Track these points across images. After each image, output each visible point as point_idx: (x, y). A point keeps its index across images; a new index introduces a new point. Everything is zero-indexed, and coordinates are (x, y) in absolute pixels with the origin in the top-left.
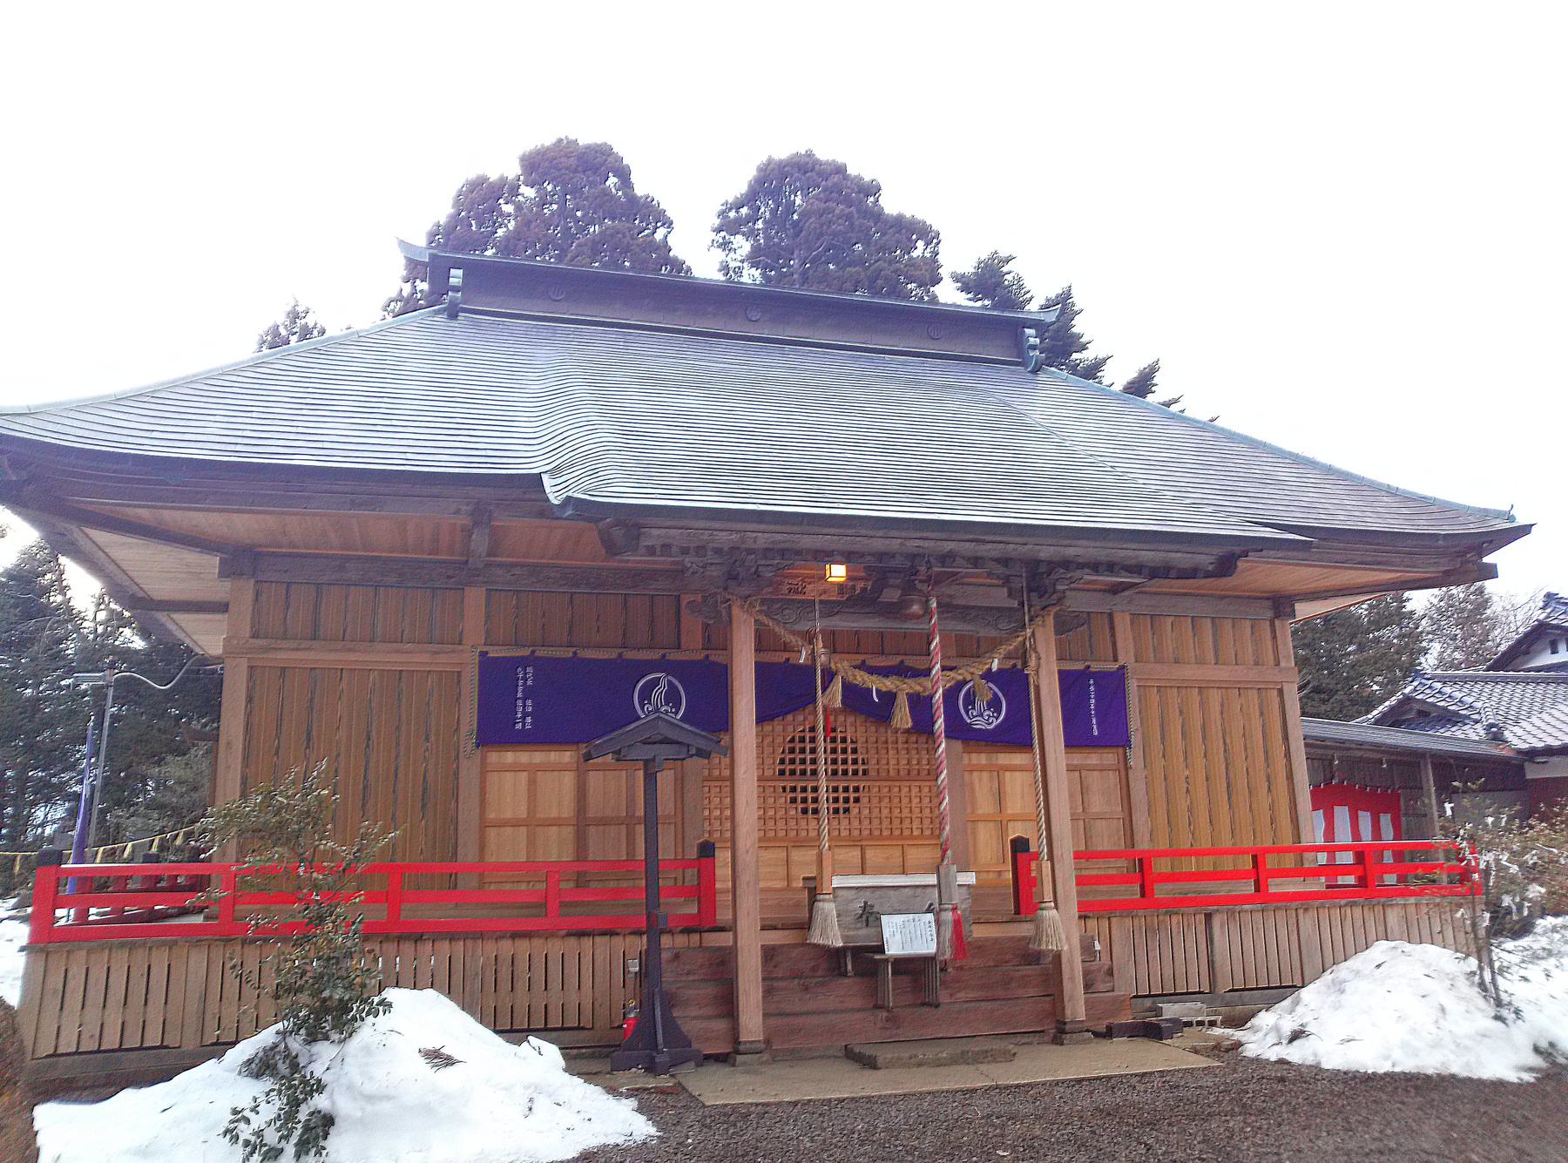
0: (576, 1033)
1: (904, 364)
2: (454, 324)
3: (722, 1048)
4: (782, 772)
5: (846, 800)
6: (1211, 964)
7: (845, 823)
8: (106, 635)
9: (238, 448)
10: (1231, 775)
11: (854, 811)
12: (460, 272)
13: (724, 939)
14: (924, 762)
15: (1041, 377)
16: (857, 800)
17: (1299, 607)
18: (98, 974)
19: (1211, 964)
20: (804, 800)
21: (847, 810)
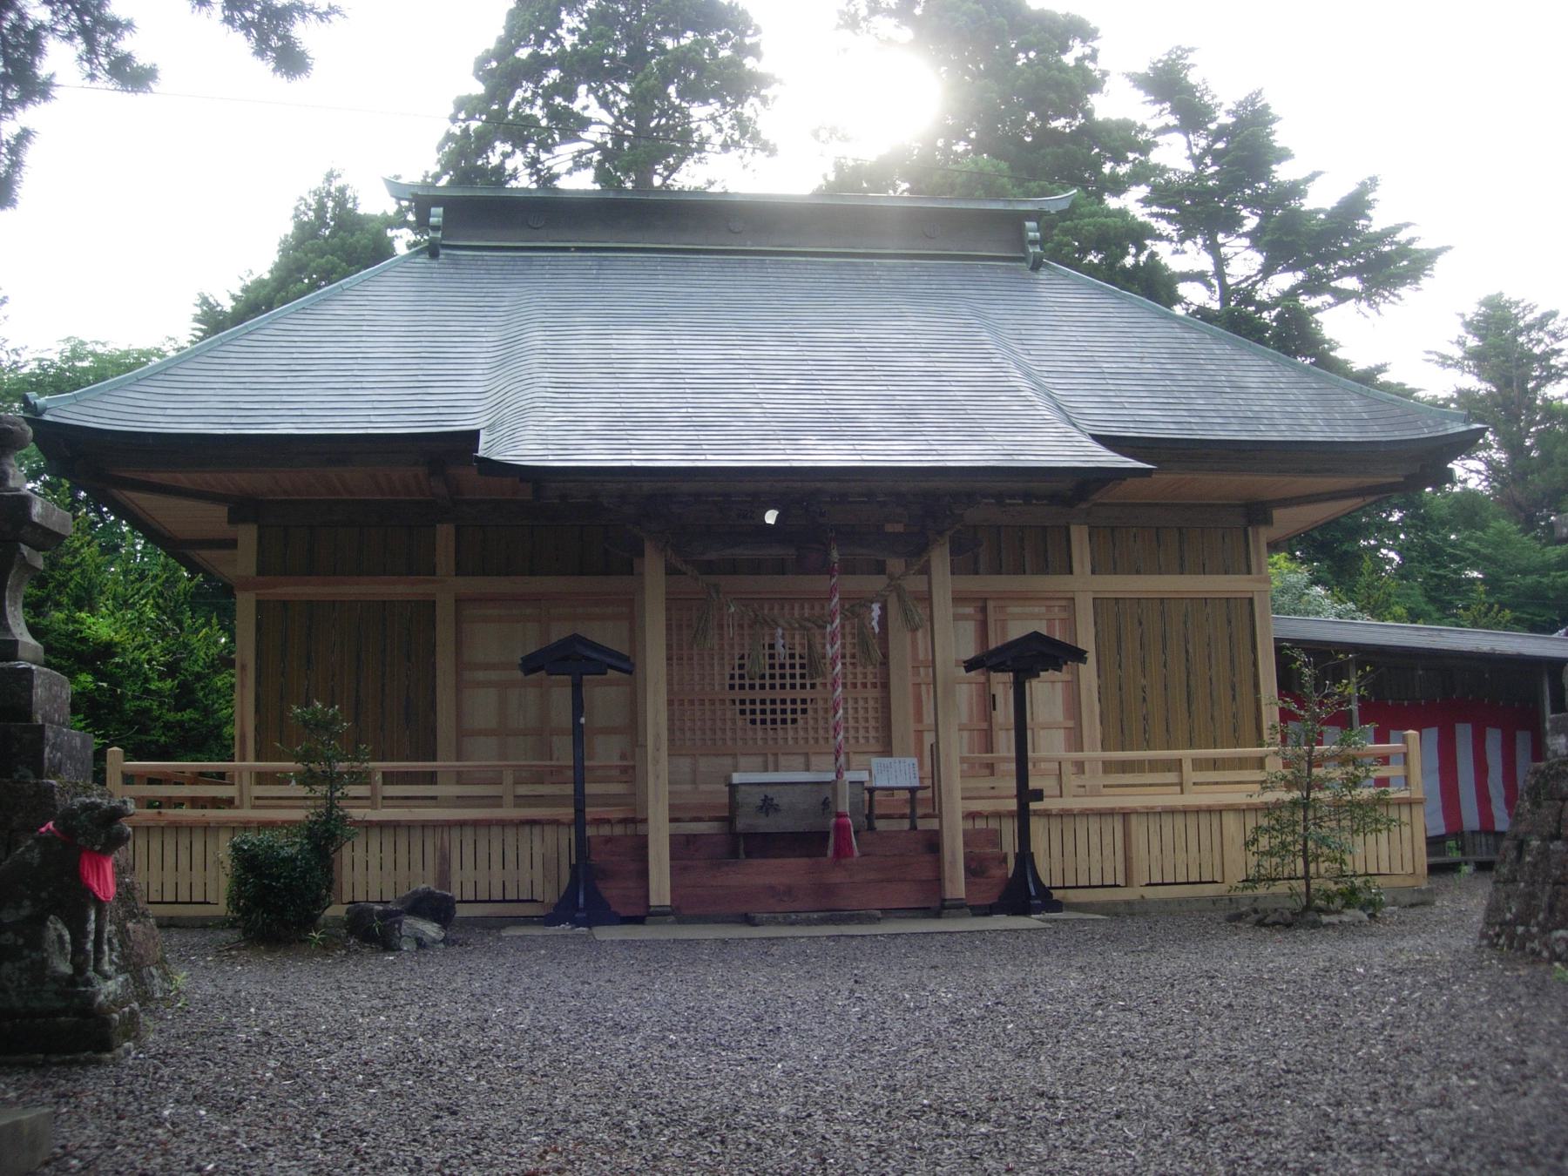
0: (1243, 958)
1: (891, 269)
2: (434, 264)
3: (639, 912)
4: (732, 687)
5: (794, 711)
6: (1127, 860)
7: (791, 734)
8: (540, 177)
9: (234, 420)
10: (1192, 683)
11: (801, 722)
12: (440, 210)
13: (933, 824)
14: (860, 676)
15: (1043, 275)
16: (804, 711)
17: (1278, 514)
18: (1082, 835)
19: (1127, 860)
20: (753, 712)
21: (794, 721)
